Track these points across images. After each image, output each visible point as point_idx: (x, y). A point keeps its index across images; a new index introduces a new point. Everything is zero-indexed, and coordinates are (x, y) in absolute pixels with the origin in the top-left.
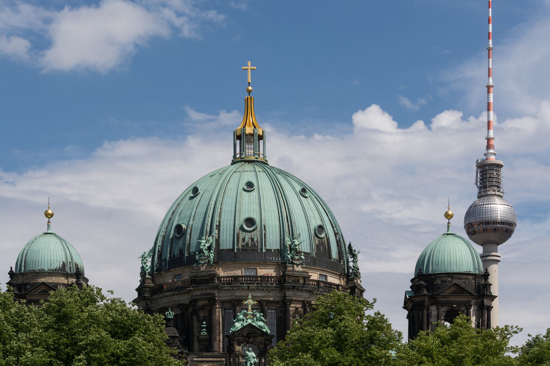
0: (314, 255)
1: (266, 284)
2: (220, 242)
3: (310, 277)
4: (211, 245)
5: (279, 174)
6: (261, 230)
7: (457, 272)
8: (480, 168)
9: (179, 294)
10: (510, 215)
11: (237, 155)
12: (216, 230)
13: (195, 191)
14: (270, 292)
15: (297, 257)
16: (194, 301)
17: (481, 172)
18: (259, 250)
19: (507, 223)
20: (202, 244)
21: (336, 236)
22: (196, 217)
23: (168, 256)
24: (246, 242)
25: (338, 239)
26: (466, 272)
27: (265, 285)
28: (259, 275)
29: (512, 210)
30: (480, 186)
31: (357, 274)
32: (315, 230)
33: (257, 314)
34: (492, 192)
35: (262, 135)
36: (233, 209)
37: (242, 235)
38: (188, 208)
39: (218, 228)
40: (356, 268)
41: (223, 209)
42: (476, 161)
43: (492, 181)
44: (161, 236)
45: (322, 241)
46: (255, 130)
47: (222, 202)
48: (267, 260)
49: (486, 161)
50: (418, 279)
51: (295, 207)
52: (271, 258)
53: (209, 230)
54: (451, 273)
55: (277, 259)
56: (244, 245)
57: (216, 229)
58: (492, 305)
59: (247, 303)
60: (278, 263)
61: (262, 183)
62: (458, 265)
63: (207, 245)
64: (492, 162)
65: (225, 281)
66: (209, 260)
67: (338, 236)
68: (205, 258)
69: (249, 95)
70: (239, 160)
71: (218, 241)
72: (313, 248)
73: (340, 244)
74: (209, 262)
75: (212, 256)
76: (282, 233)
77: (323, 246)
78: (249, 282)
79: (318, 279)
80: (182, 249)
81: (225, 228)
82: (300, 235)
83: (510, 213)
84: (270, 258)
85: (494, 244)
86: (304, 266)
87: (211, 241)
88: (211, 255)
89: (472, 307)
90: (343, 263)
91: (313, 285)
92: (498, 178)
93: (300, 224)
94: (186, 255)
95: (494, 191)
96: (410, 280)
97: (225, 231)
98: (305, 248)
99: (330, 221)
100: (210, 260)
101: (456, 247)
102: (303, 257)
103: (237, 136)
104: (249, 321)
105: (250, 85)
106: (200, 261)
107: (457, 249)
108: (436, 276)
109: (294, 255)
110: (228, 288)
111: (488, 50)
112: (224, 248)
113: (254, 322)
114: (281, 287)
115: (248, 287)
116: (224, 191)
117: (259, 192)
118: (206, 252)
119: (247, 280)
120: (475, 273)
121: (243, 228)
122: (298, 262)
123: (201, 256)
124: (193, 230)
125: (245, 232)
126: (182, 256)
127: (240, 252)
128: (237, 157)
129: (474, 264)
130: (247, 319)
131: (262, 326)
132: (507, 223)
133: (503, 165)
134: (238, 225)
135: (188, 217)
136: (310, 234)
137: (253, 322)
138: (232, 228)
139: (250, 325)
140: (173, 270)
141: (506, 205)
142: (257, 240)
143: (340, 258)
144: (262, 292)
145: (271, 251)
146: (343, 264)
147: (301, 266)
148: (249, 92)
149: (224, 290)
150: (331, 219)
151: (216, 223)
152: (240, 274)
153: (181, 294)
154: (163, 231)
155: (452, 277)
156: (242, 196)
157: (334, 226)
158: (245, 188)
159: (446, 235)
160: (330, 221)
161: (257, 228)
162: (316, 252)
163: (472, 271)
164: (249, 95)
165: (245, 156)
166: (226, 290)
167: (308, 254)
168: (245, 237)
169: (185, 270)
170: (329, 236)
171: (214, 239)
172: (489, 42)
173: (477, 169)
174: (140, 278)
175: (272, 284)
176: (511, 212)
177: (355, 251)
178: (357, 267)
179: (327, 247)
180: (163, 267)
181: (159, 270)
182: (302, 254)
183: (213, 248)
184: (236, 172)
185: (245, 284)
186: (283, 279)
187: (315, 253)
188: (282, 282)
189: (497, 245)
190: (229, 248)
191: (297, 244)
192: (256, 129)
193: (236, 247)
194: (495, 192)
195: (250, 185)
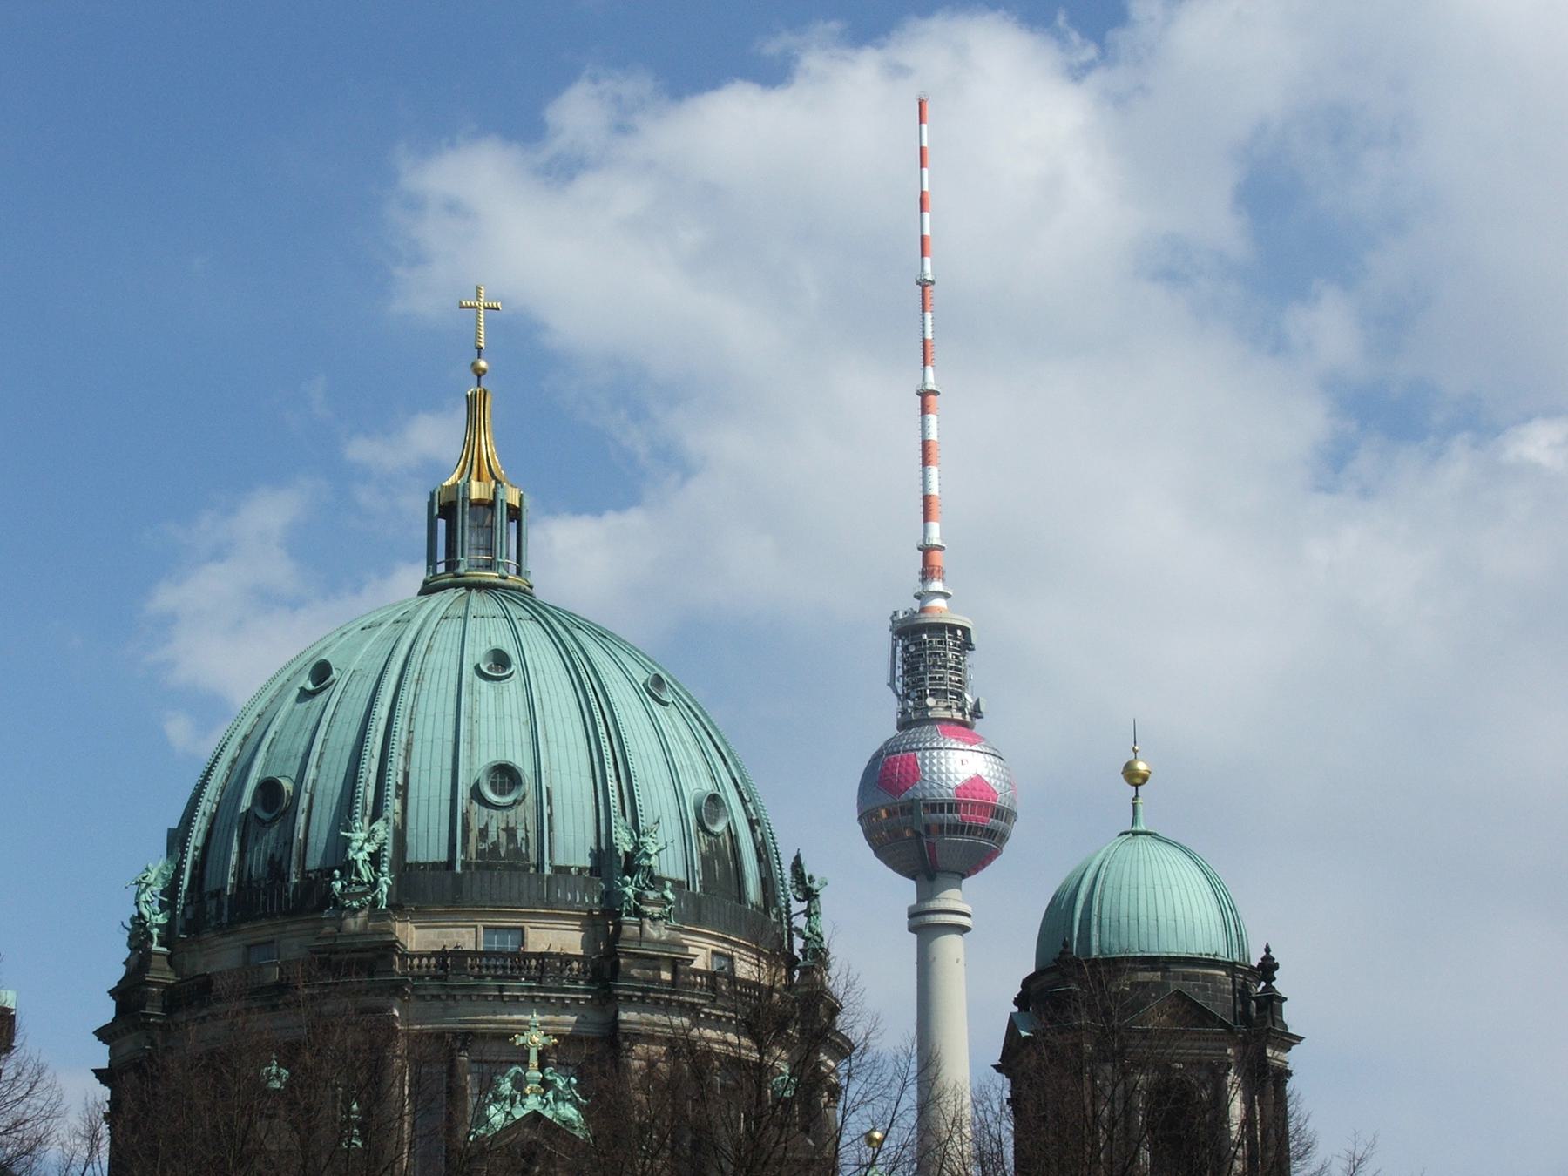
0: (698, 890)
1: (556, 981)
2: (408, 839)
3: (692, 961)
4: (382, 846)
5: (580, 628)
6: (539, 803)
7: (1179, 955)
8: (903, 637)
9: (269, 1009)
10: (1003, 785)
11: (438, 566)
12: (396, 800)
13: (322, 672)
15: (652, 895)
17: (905, 649)
18: (532, 870)
19: (946, 806)
20: (355, 845)
21: (753, 830)
22: (327, 758)
23: (231, 880)
25: (760, 838)
26: (1206, 954)
27: (551, 985)
28: (530, 949)
29: (1004, 770)
30: (903, 692)
31: (818, 956)
32: (698, 809)
33: (558, 1079)
34: (941, 713)
35: (518, 505)
36: (450, 735)
37: (479, 817)
38: (296, 727)
39: (401, 793)
40: (818, 935)
41: (417, 735)
42: (891, 614)
43: (941, 679)
44: (204, 813)
45: (717, 844)
46: (500, 491)
47: (412, 711)
48: (558, 900)
49: (922, 615)
50: (1054, 976)
51: (636, 732)
52: (569, 895)
53: (372, 800)
54: (1162, 957)
55: (587, 901)
56: (485, 849)
58: (1289, 1067)
59: (525, 1042)
60: (591, 912)
61: (534, 653)
62: (1181, 932)
63: (369, 848)
64: (941, 621)
65: (425, 969)
66: (376, 896)
67: (759, 831)
68: (360, 889)
69: (479, 386)
70: (448, 580)
71: (400, 835)
72: (693, 866)
73: (768, 856)
74: (375, 902)
75: (385, 881)
76: (602, 816)
77: (721, 860)
78: (500, 972)
79: (707, 967)
80: (277, 859)
81: (424, 794)
82: (658, 822)
83: (999, 778)
84: (567, 896)
85: (950, 875)
86: (674, 923)
87: (381, 837)
88: (382, 879)
89: (1232, 1070)
90: (776, 916)
91: (698, 987)
92: (960, 670)
93: (654, 788)
94: (294, 879)
95: (949, 708)
96: (1279, 970)
97: (424, 804)
98: (672, 866)
99: (734, 780)
100: (379, 896)
101: (1171, 875)
102: (671, 896)
104: (533, 1103)
105: (482, 356)
106: (347, 901)
107: (1173, 882)
108: (1116, 965)
109: (643, 888)
110: (435, 992)
111: (920, 288)
112: (422, 859)
113: (548, 1108)
114: (606, 991)
115: (501, 989)
116: (416, 675)
117: (528, 685)
118: (366, 872)
119: (495, 967)
120: (1230, 960)
121: (481, 794)
122: (656, 910)
123: (350, 884)
124: (317, 800)
125: (487, 807)
126: (279, 882)
127: (472, 873)
128: (438, 572)
129: (1227, 932)
130: (525, 1096)
131: (571, 1119)
132: (946, 806)
133: (970, 627)
134: (467, 785)
135: (300, 755)
136: (683, 819)
137: (545, 1106)
138: (447, 795)
139: (536, 1116)
140: (244, 926)
141: (986, 753)
142: (527, 836)
143: (765, 899)
144: (543, 1007)
145: (570, 873)
146: (775, 920)
147: (666, 924)
148: (479, 373)
149: (423, 997)
150: (737, 776)
151: (395, 778)
152: (470, 946)
153: (274, 1008)
154: (209, 801)
155: (1165, 970)
156: (474, 692)
157: (747, 798)
158: (484, 668)
159: (1131, 835)
160: (734, 780)
161: (524, 797)
162: (701, 878)
163: (1223, 954)
164: (479, 386)
165: (466, 571)
166: (429, 998)
168: (487, 825)
169: (289, 928)
170: (736, 830)
171: (390, 830)
173: (893, 639)
174: (126, 953)
175: (576, 982)
176: (997, 775)
177: (811, 879)
178: (819, 930)
179: (731, 863)
180: (208, 916)
181: (195, 926)
182: (668, 884)
183: (385, 859)
184: (446, 618)
185: (489, 979)
186: (607, 965)
187: (700, 882)
188: (607, 974)
189: (960, 878)
190: (436, 860)
191: (655, 851)
192: (502, 487)
193: (459, 857)
194: (949, 713)
195: (500, 659)
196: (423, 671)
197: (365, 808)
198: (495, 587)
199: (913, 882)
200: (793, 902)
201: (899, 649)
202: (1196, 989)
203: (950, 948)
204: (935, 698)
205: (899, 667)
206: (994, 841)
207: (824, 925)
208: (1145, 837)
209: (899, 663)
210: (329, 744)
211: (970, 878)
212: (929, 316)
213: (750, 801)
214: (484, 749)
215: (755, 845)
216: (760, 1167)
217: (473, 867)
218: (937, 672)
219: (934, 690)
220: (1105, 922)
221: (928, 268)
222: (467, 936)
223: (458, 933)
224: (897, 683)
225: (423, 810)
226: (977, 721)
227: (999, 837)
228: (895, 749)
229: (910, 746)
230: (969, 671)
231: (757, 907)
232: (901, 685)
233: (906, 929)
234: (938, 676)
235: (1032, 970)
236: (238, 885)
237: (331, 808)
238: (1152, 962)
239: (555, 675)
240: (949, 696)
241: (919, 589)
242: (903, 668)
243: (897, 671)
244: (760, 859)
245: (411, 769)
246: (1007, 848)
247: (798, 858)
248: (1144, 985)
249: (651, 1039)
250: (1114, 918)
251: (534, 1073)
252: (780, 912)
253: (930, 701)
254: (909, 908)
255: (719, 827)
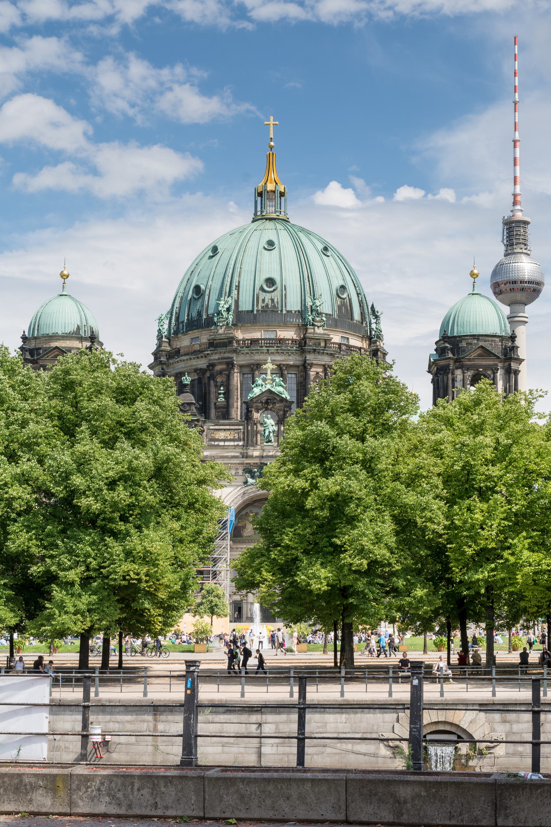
4: (230, 306)
13: (215, 250)
14: (290, 355)
15: (318, 319)
16: (212, 366)
17: (507, 229)
18: (279, 312)
20: (221, 305)
21: (358, 297)
22: (215, 277)
23: (186, 318)
24: (266, 303)
32: (337, 290)
36: (253, 269)
37: (262, 295)
45: (344, 302)
57: (236, 289)
58: (520, 369)
62: (484, 327)
68: (223, 320)
71: (237, 302)
74: (228, 324)
75: (231, 318)
78: (268, 345)
81: (245, 289)
86: (325, 328)
94: (204, 317)
95: (521, 249)
103: (258, 193)
104: (269, 387)
118: (225, 314)
119: (267, 343)
122: (319, 324)
129: (501, 326)
130: (266, 384)
136: (331, 294)
140: (190, 332)
148: (271, 148)
150: (353, 279)
151: (235, 283)
158: (266, 247)
161: (277, 288)
163: (499, 333)
167: (330, 315)
171: (233, 300)
172: (515, 95)
177: (378, 312)
181: (176, 333)
182: (324, 315)
186: (303, 342)
188: (303, 345)
193: (255, 308)
195: (271, 243)
197: (226, 293)
198: (275, 219)
200: (372, 320)
209: (505, 233)
210: (216, 273)
220: (459, 324)
235: (438, 339)
236: (188, 319)
238: (474, 336)
241: (512, 208)
250: (462, 322)
251: (269, 377)
255: (345, 296)
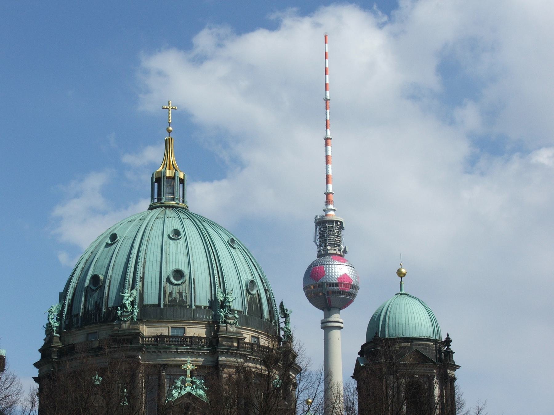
0: (247, 314)
1: (196, 346)
2: (144, 296)
3: (245, 339)
4: (135, 298)
5: (205, 222)
6: (190, 283)
7: (417, 337)
8: (319, 225)
9: (95, 356)
10: (354, 277)
11: (155, 200)
12: (140, 282)
13: (114, 237)
15: (230, 316)
17: (320, 229)
18: (188, 307)
19: (334, 284)
20: (126, 298)
21: (266, 293)
22: (115, 267)
23: (82, 311)
25: (268, 296)
26: (426, 337)
27: (195, 348)
28: (187, 335)
29: (355, 272)
30: (319, 244)
31: (289, 337)
32: (247, 286)
33: (197, 381)
34: (333, 252)
35: (183, 178)
36: (159, 260)
37: (169, 288)
38: (105, 257)
39: (142, 280)
40: (289, 330)
41: (147, 259)
42: (315, 217)
43: (333, 239)
44: (72, 287)
45: (254, 298)
46: (177, 173)
47: (146, 251)
48: (197, 318)
49: (326, 217)
50: (372, 344)
51: (225, 258)
52: (201, 316)
53: (131, 282)
54: (411, 338)
55: (207, 318)
56: (171, 300)
58: (455, 377)
59: (185, 368)
60: (209, 322)
61: (189, 231)
62: (417, 329)
63: (131, 299)
64: (332, 219)
65: (150, 342)
66: (133, 316)
67: (268, 293)
68: (127, 314)
69: (169, 136)
70: (158, 205)
71: (141, 295)
72: (245, 306)
73: (271, 302)
74: (132, 318)
75: (136, 311)
76: (213, 288)
77: (255, 303)
78: (177, 343)
79: (250, 341)
80: (98, 303)
81: (150, 280)
82: (233, 290)
83: (353, 275)
84: (200, 316)
85: (336, 309)
86: (238, 326)
87: (135, 295)
88: (135, 310)
89: (435, 378)
90: (274, 323)
91: (247, 348)
92: (339, 236)
93: (231, 278)
94: (104, 310)
95: (335, 250)
96: (452, 342)
97: (150, 284)
98: (237, 306)
99: (259, 275)
100: (134, 316)
101: (414, 309)
102: (237, 316)
104: (188, 389)
105: (170, 126)
106: (123, 318)
107: (415, 311)
108: (394, 341)
109: (227, 314)
110: (154, 350)
111: (325, 102)
112: (149, 303)
113: (194, 391)
114: (214, 350)
115: (177, 349)
116: (147, 238)
117: (187, 242)
118: (129, 308)
119: (175, 341)
120: (435, 339)
121: (170, 280)
122: (232, 321)
123: (124, 312)
124: (112, 282)
125: (172, 285)
126: (99, 311)
127: (167, 308)
128: (155, 202)
129: (433, 329)
130: (185, 387)
131: (202, 395)
132: (334, 284)
133: (343, 221)
134: (165, 277)
135: (106, 266)
136: (241, 289)
137: (193, 390)
138: (158, 280)
139: (189, 394)
140: (86, 327)
141: (348, 266)
142: (186, 295)
143: (270, 317)
144: (192, 355)
145: (201, 308)
146: (274, 325)
147: (235, 326)
148: (169, 132)
149: (149, 352)
150: (260, 274)
151: (140, 274)
152: (166, 334)
153: (97, 356)
154: (74, 283)
155: (412, 342)
156: (168, 244)
157: (264, 282)
158: (171, 236)
159: (400, 295)
160: (259, 275)
161: (185, 281)
162: (248, 310)
163: (432, 337)
164: (169, 136)
165: (165, 201)
166: (151, 352)
168: (172, 291)
169: (102, 327)
170: (260, 293)
171: (138, 293)
173: (315, 225)
174: (44, 336)
175: (203, 347)
176: (352, 274)
177: (287, 310)
178: (289, 328)
179: (258, 305)
180: (73, 323)
181: (69, 327)
182: (236, 312)
183: (136, 303)
184: (158, 218)
185: (173, 345)
186: (215, 341)
187: (247, 311)
188: (214, 344)
189: (339, 310)
190: (154, 303)
191: (231, 300)
192: (177, 172)
193: (162, 302)
194: (335, 251)
195: (177, 233)
196: (149, 237)
197: (129, 285)
198: (175, 207)
199: (323, 311)
200: (280, 318)
201: (318, 229)
202: (423, 349)
203: (336, 334)
204: (330, 246)
205: (318, 236)
206: (351, 297)
207: (291, 326)
208: (405, 295)
209: (318, 234)
210: (116, 262)
211: (343, 310)
212: (328, 111)
213: (265, 283)
214: (171, 264)
215: (267, 298)
216: (269, 412)
217: (167, 306)
218: (331, 237)
219: (330, 243)
220: (391, 325)
221: (328, 94)
222: (165, 330)
223: (162, 329)
224: (317, 241)
225: (149, 286)
226: (345, 254)
227: (353, 295)
228: (316, 264)
229: (322, 263)
230: (342, 237)
231: (267, 320)
232: (318, 242)
233: (320, 328)
234: (331, 238)
235: (365, 342)
236: (84, 312)
237: (117, 285)
238: (407, 340)
239: (196, 238)
240: (335, 246)
241: (325, 208)
242: (319, 236)
243: (317, 237)
244: (268, 303)
245: (145, 272)
246: (356, 299)
247: (282, 303)
248: (404, 347)
249: (230, 367)
250: (394, 324)
251: (189, 379)
252: (276, 322)
253: (329, 248)
254: (321, 321)
255: (254, 292)
